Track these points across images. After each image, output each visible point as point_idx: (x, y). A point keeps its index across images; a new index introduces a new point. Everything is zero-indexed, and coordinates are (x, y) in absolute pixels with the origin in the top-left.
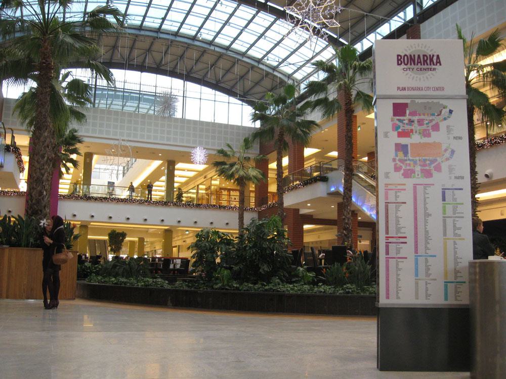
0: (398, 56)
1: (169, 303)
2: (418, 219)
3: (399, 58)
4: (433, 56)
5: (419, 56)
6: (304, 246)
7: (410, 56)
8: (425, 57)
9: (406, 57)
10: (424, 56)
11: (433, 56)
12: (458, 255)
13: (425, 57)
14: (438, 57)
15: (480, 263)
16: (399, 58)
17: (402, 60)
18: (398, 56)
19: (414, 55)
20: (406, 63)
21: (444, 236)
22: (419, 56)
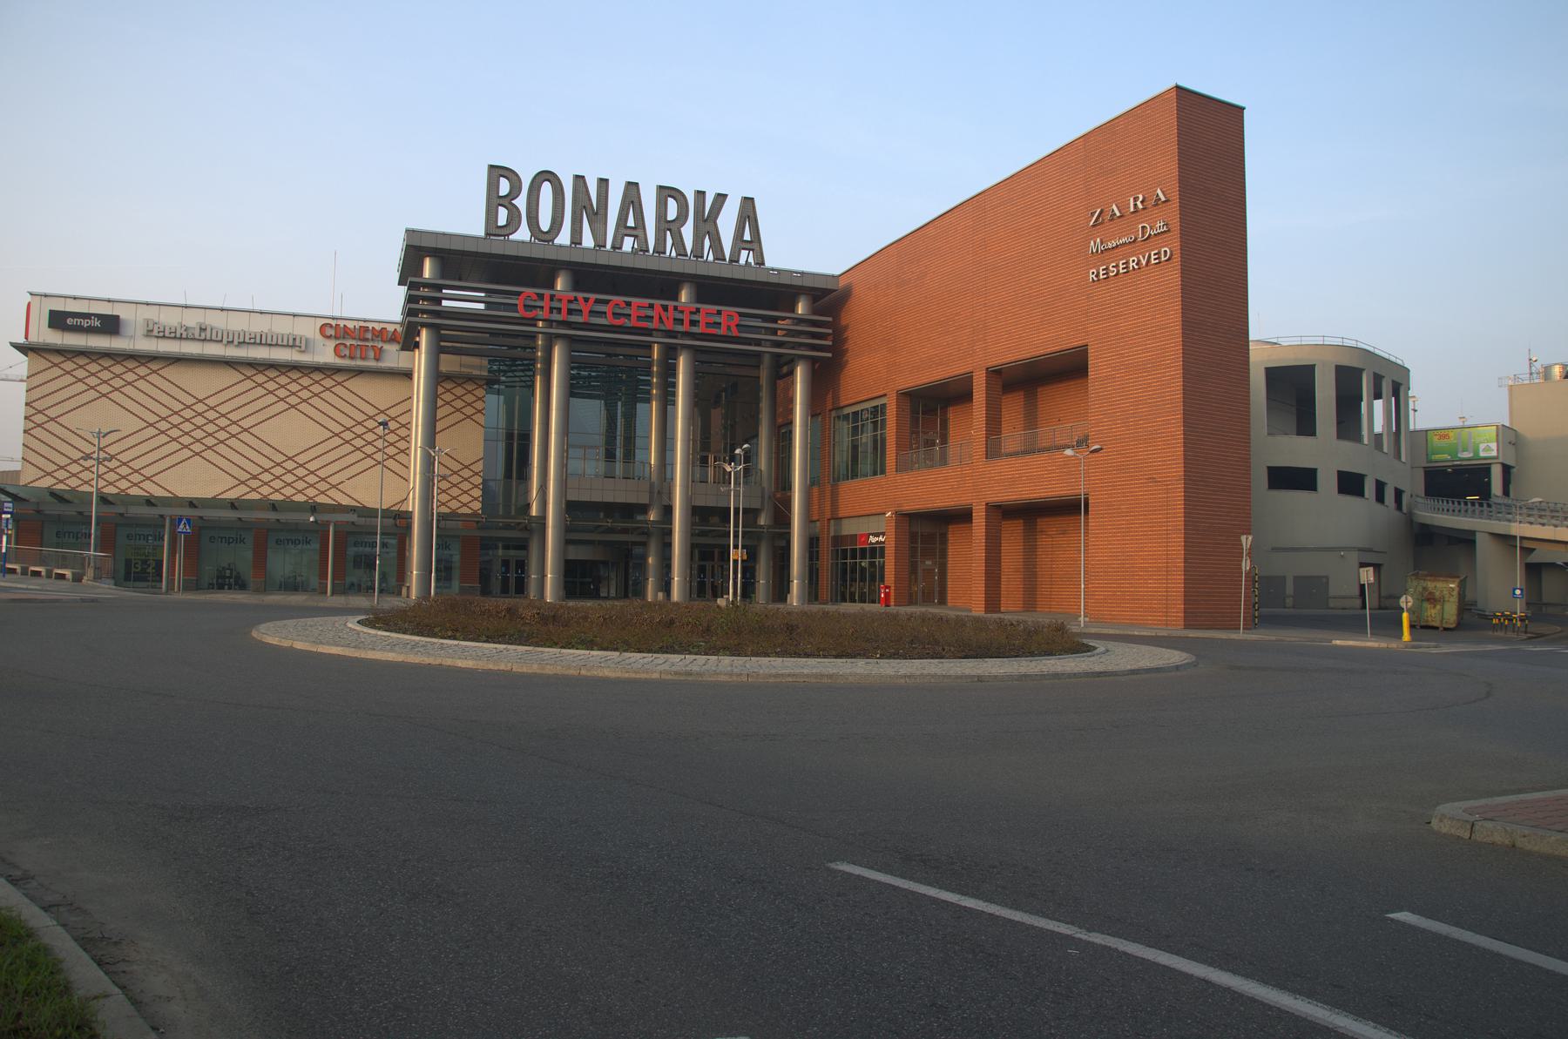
0: (496, 172)
1: (789, 494)
2: (1134, 667)
3: (504, 187)
4: (721, 198)
5: (632, 188)
6: (113, 578)
7: (579, 180)
8: (672, 204)
9: (546, 189)
10: (665, 193)
11: (721, 198)
12: (1377, 607)
13: (672, 204)
14: (748, 210)
15: (92, 516)
16: (504, 187)
17: (521, 202)
18: (496, 172)
19: (603, 183)
20: (546, 189)
21: (995, 374)
22: (632, 188)
